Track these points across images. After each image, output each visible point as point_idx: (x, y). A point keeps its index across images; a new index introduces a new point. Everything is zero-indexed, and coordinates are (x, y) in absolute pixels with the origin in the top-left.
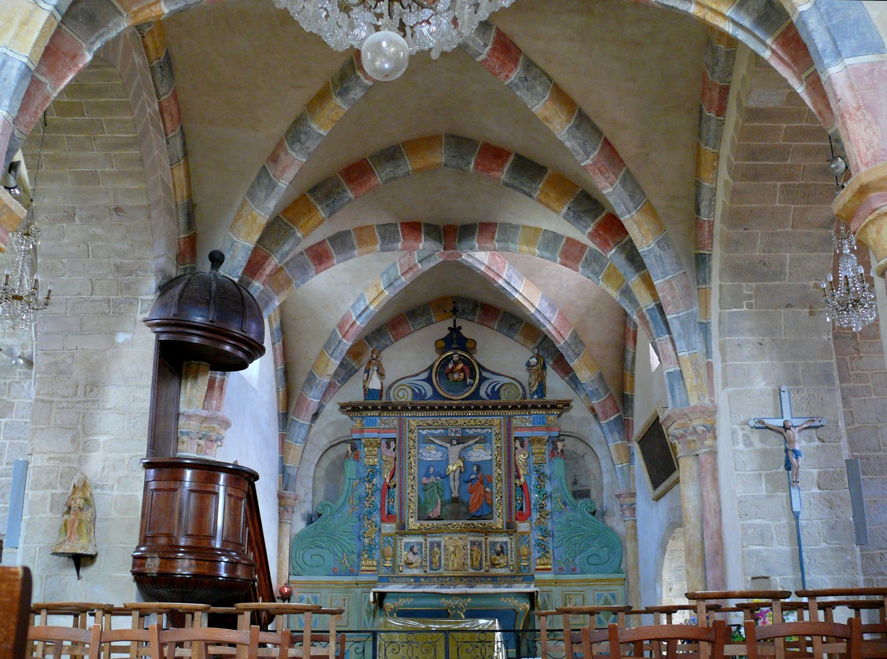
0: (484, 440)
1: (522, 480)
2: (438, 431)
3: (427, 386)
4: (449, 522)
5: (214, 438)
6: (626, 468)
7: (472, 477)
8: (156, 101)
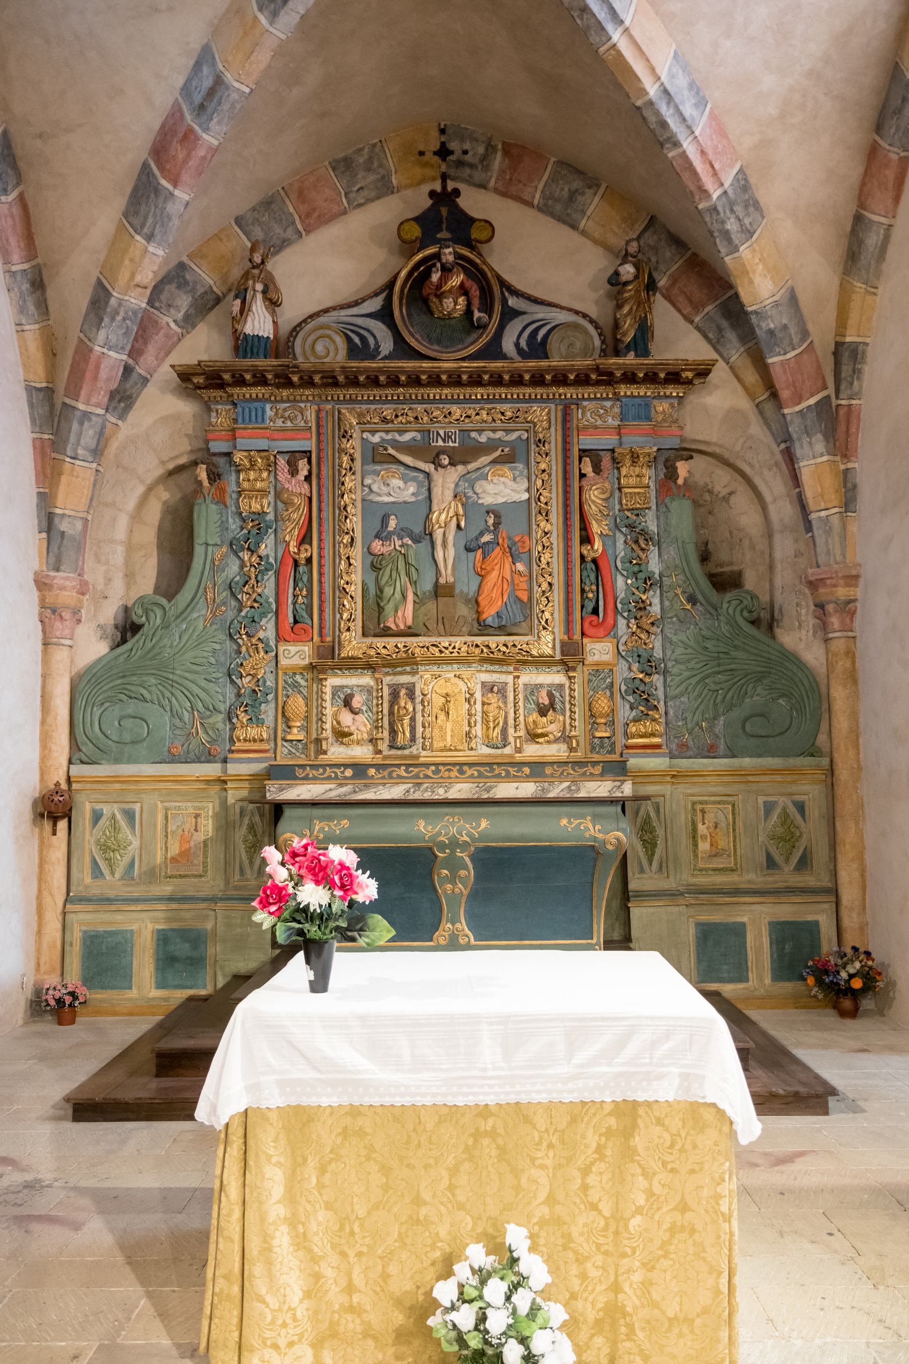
1: (598, 545)
2: (407, 437)
3: (379, 329)
4: (433, 640)
6: (835, 520)
7: (487, 538)
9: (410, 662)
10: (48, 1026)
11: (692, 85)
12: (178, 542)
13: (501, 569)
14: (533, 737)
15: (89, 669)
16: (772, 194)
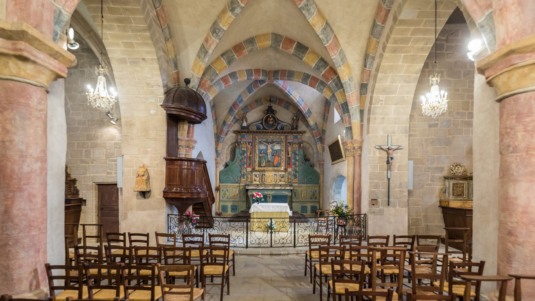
0: (278, 143)
3: (261, 125)
5: (191, 147)
8: (155, 10)
9: (264, 171)
12: (233, 153)
13: (277, 158)
14: (280, 181)
16: (313, 111)
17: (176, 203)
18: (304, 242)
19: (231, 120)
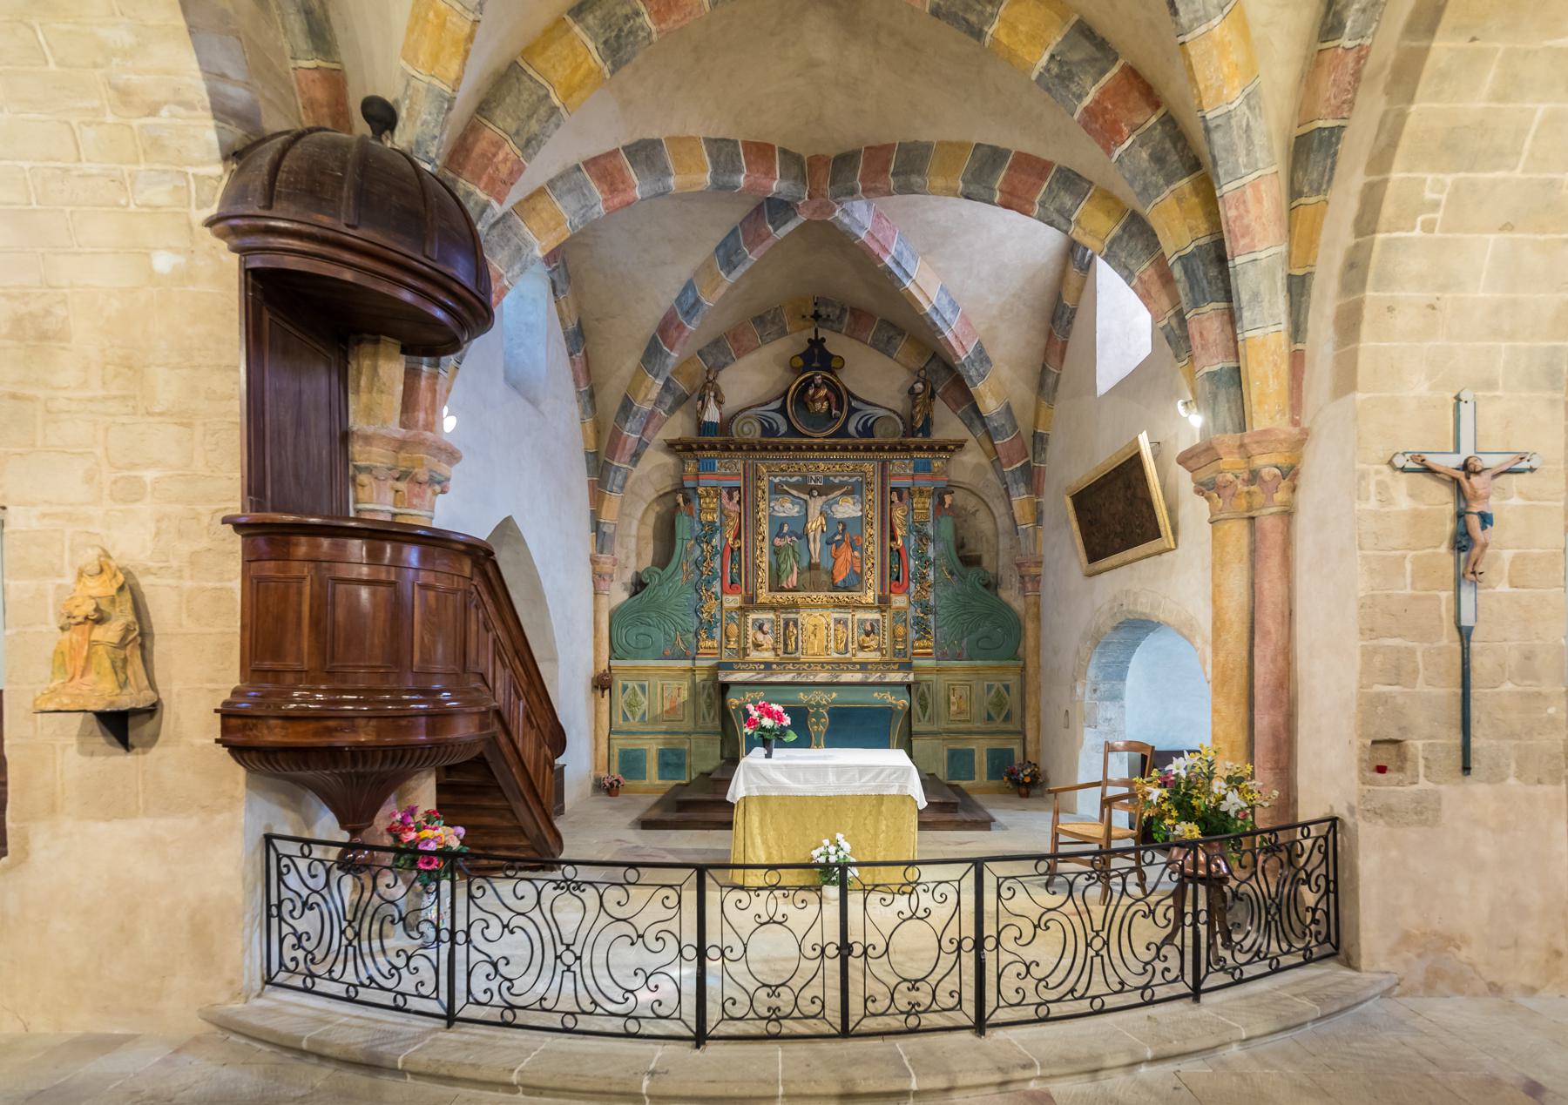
3: (779, 418)
5: (423, 475)
9: (794, 606)
10: (603, 796)
11: (952, 302)
12: (666, 535)
13: (846, 554)
14: (862, 648)
15: (619, 608)
16: (994, 354)
17: (325, 776)
18: (1032, 998)
19: (653, 394)
